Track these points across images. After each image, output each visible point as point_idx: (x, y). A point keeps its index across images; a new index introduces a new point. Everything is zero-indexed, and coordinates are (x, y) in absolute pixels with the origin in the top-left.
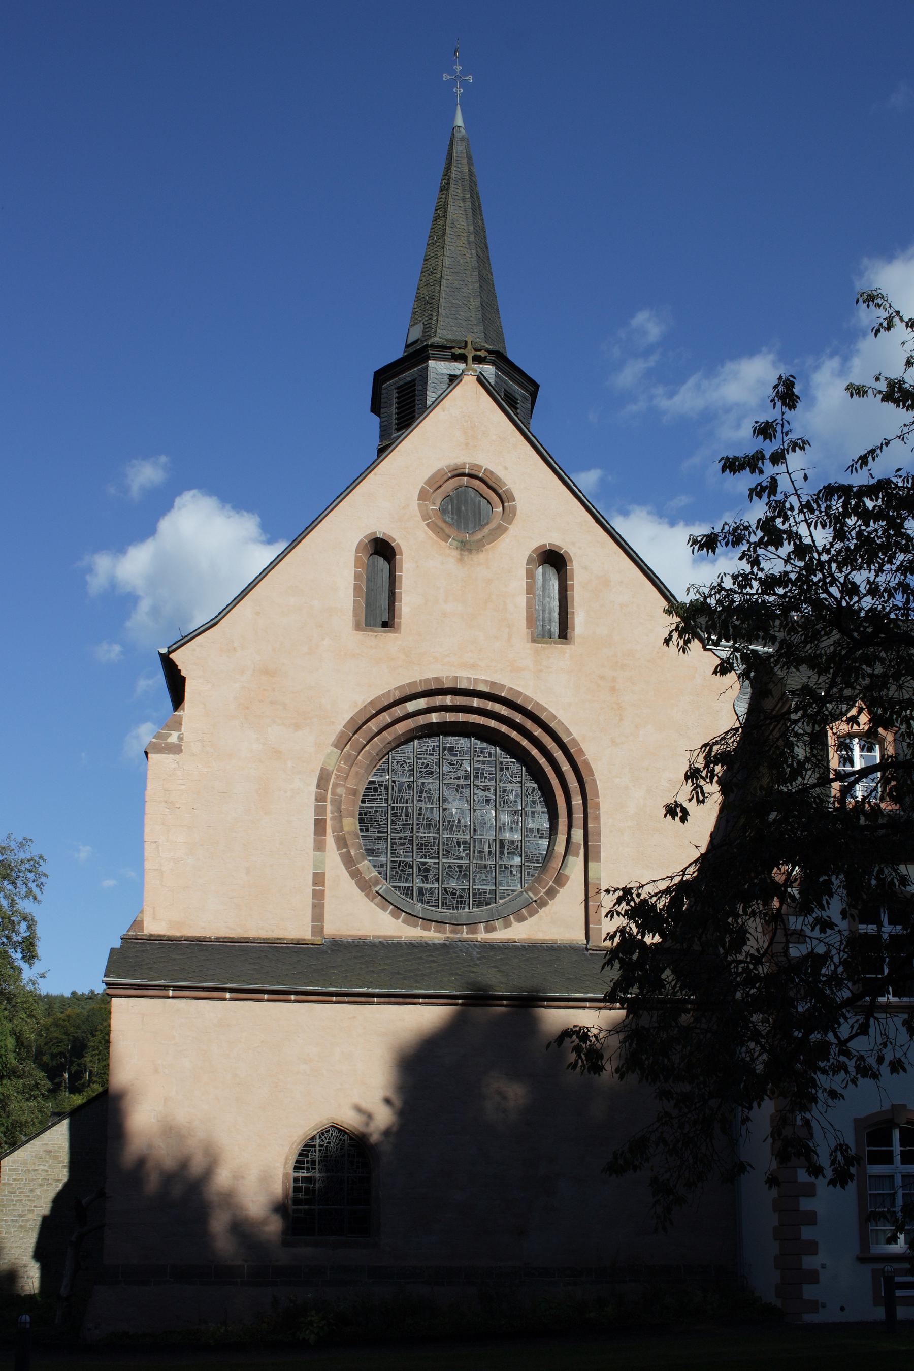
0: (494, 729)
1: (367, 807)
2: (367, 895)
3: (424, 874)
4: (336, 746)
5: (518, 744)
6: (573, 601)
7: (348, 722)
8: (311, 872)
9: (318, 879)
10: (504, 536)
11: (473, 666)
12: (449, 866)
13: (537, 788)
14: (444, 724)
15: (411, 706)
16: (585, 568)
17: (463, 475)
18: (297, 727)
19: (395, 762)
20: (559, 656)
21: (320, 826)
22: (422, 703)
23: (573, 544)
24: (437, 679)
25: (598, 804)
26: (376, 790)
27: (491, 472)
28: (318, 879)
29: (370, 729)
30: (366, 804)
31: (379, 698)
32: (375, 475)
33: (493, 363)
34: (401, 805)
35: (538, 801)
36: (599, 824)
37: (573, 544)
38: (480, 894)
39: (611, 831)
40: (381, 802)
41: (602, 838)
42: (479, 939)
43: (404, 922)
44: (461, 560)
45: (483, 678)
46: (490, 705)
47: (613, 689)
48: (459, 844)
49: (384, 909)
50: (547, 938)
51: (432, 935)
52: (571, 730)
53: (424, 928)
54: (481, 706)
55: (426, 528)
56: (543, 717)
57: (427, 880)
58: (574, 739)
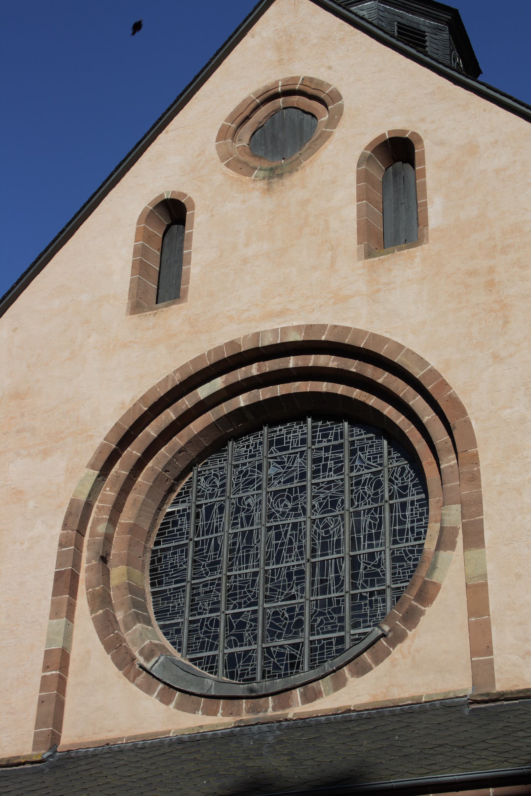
0: (327, 394)
2: (126, 675)
3: (238, 632)
4: (92, 466)
6: (425, 190)
7: (111, 431)
8: (43, 649)
10: (327, 143)
11: (281, 313)
12: (276, 613)
13: (407, 467)
14: (254, 407)
15: (203, 392)
16: (442, 143)
17: (276, 96)
18: (45, 454)
20: (405, 266)
21: (66, 582)
22: (218, 384)
24: (232, 344)
26: (175, 523)
27: (311, 79)
28: (59, 662)
29: (148, 434)
30: (162, 546)
31: (154, 389)
32: (167, 133)
34: (210, 536)
35: (410, 485)
36: (480, 486)
37: (423, 120)
38: (322, 648)
39: (500, 493)
40: (181, 539)
41: (485, 508)
43: (179, 707)
44: (269, 190)
45: (295, 324)
47: (491, 285)
48: (289, 576)
49: (149, 691)
50: (406, 695)
51: (219, 720)
52: (427, 359)
53: (208, 712)
54: (301, 364)
56: (383, 352)
57: (241, 640)
58: (432, 371)
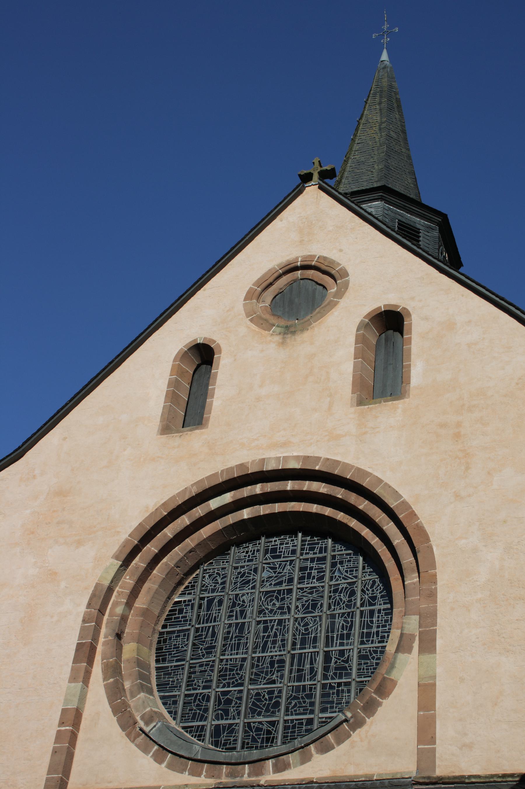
1: (168, 633)
2: (128, 735)
5: (345, 526)
9: (73, 719)
12: (258, 694)
13: (377, 581)
15: (214, 504)
16: (426, 319)
18: (79, 543)
19: (207, 576)
20: (389, 415)
21: (85, 653)
22: (227, 498)
23: (413, 299)
25: (435, 576)
26: (181, 611)
27: (325, 258)
28: (73, 719)
29: (166, 535)
30: (168, 629)
32: (205, 290)
33: (381, 199)
35: (379, 596)
36: (436, 602)
37: (413, 299)
39: (452, 609)
40: (185, 625)
41: (439, 620)
42: (262, 782)
43: (170, 766)
44: (283, 343)
45: (295, 454)
46: (307, 486)
47: (457, 436)
48: (272, 663)
49: (146, 751)
50: (361, 773)
52: (401, 492)
54: (297, 488)
55: (249, 323)
56: (366, 483)
57: (227, 714)
